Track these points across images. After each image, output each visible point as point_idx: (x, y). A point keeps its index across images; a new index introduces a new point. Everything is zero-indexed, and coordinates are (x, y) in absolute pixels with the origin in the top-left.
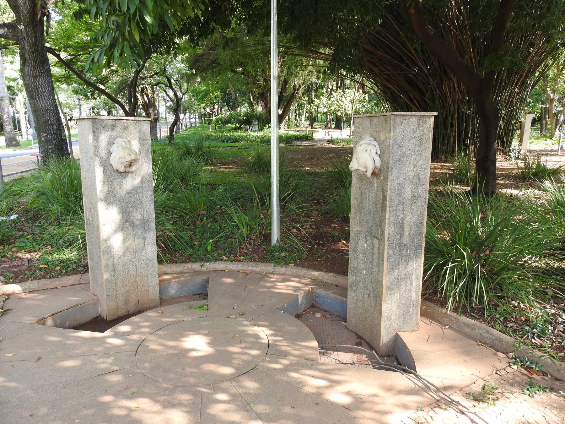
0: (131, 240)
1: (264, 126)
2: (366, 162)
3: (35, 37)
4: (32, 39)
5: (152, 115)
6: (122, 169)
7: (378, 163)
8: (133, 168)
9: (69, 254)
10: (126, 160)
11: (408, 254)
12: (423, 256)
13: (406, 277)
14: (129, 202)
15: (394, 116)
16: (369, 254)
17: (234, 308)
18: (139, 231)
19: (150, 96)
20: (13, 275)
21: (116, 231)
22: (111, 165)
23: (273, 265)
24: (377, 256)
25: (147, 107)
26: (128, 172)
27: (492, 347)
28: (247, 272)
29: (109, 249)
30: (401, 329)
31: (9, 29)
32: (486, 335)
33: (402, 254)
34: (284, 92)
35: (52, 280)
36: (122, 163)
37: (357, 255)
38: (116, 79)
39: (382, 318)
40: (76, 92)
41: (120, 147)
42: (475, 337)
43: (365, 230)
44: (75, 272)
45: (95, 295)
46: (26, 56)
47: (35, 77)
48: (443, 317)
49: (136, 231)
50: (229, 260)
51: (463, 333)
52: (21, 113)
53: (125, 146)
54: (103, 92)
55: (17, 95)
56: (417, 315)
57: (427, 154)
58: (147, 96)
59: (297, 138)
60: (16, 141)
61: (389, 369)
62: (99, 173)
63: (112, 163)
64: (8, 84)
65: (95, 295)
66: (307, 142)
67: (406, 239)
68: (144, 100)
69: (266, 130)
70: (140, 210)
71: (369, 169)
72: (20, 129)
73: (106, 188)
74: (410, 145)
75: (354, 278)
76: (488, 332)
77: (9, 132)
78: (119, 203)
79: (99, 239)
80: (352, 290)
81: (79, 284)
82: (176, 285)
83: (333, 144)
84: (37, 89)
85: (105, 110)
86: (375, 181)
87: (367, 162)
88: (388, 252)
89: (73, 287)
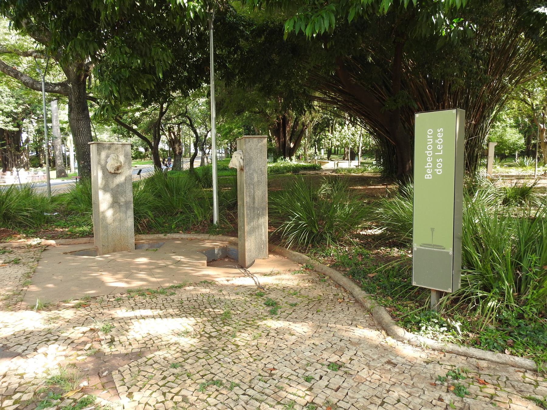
0: (118, 214)
1: (278, 158)
3: (79, 92)
4: (77, 94)
5: (177, 149)
6: (113, 171)
8: (120, 171)
9: (86, 228)
12: (267, 215)
13: (259, 227)
14: (26, 115)
18: (123, 209)
19: (176, 133)
21: (109, 208)
25: (174, 143)
26: (117, 174)
29: (104, 218)
30: (257, 257)
31: (62, 87)
34: (296, 128)
36: (113, 168)
38: (147, 120)
39: (246, 251)
40: (114, 132)
44: (87, 236)
46: (73, 106)
47: (78, 120)
49: (122, 209)
52: (70, 150)
54: (135, 132)
55: (69, 135)
56: (71, 143)
58: (174, 134)
59: (305, 168)
60: (65, 173)
62: (100, 174)
64: (61, 126)
66: (315, 171)
67: (256, 205)
68: (171, 137)
69: (279, 161)
70: (124, 196)
72: (69, 164)
73: (104, 182)
74: (255, 153)
77: (59, 165)
78: (111, 191)
79: (99, 211)
82: (147, 245)
83: (336, 173)
84: (79, 129)
85: (142, 147)
88: (247, 212)
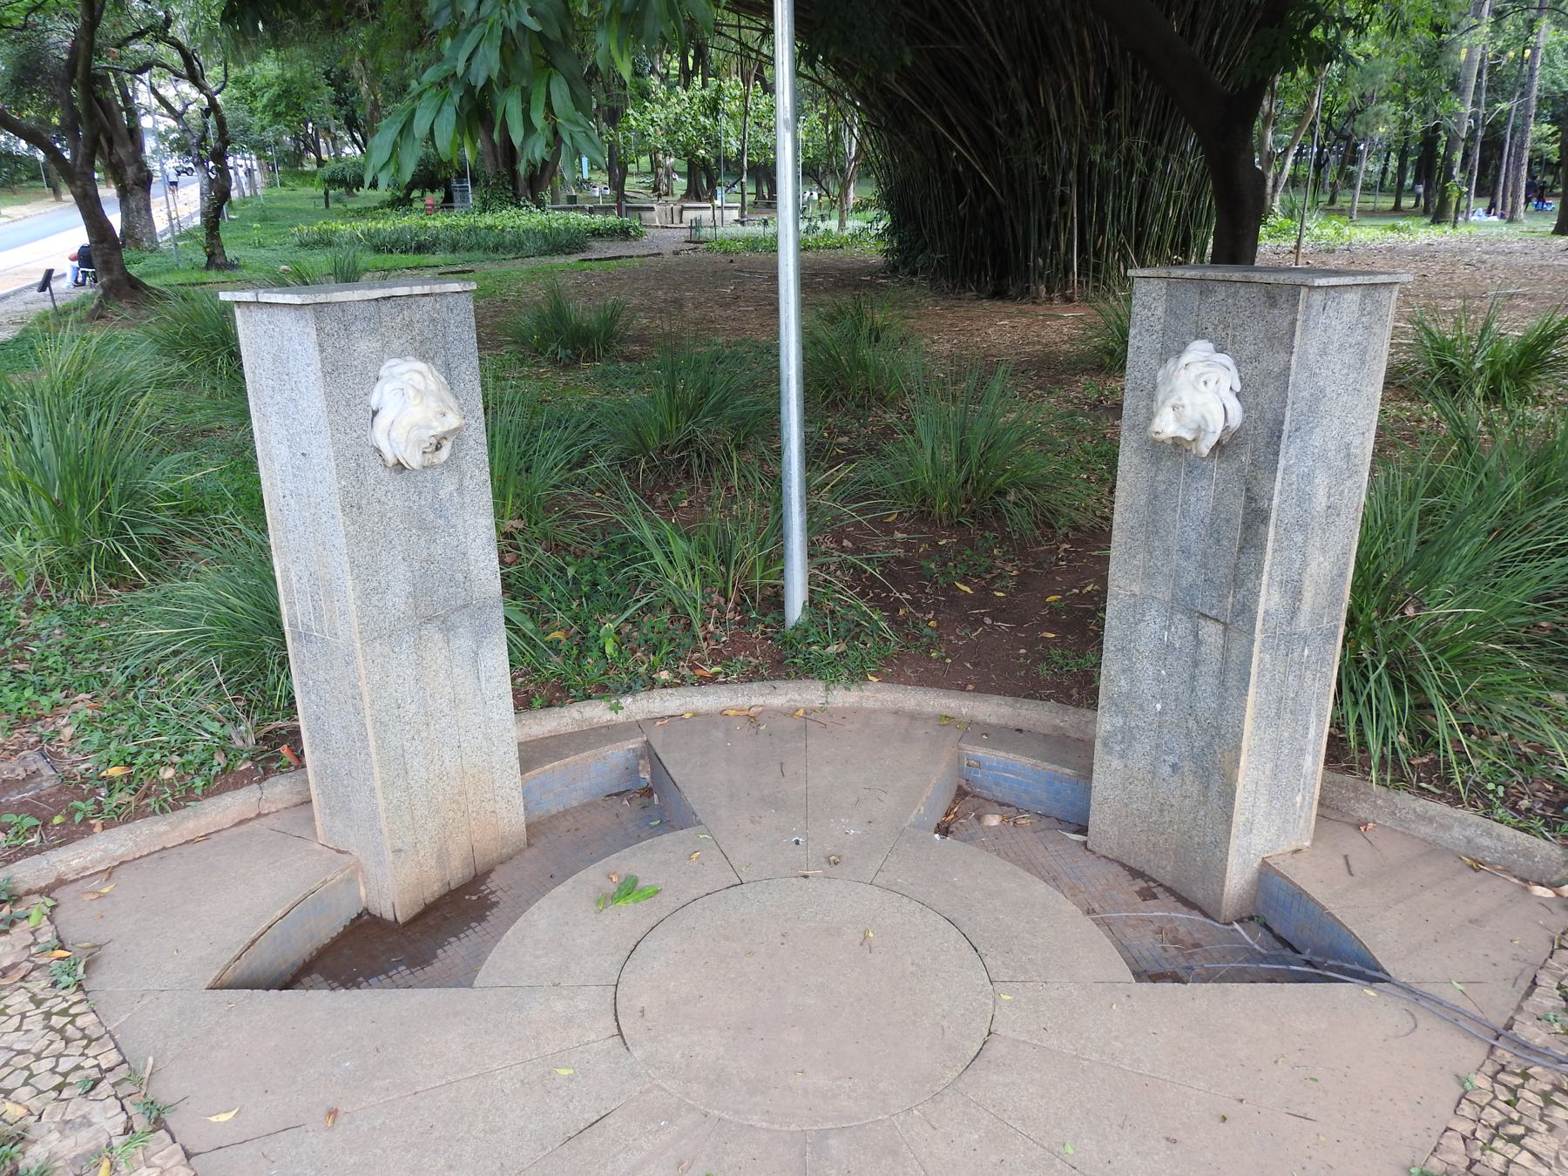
2: (1203, 417)
7: (1236, 417)
10: (432, 432)
11: (1304, 660)
15: (1306, 290)
16: (1178, 659)
17: (797, 842)
20: (35, 822)
22: (378, 450)
23: (820, 685)
24: (1216, 667)
27: (1507, 870)
28: (751, 713)
32: (1486, 842)
33: (1292, 659)
35: (173, 817)
37: (1130, 659)
41: (411, 392)
42: (1451, 847)
43: (1164, 594)
45: (339, 851)
48: (1350, 799)
50: (680, 682)
51: (1414, 837)
53: (422, 387)
57: (1372, 390)
61: (1320, 975)
63: (384, 445)
65: (339, 851)
67: (1303, 622)
71: (1210, 436)
75: (1119, 721)
76: (1489, 834)
80: (1110, 753)
81: (259, 815)
86: (1216, 469)
87: (1209, 417)
88: (1261, 660)
89: (243, 828)
